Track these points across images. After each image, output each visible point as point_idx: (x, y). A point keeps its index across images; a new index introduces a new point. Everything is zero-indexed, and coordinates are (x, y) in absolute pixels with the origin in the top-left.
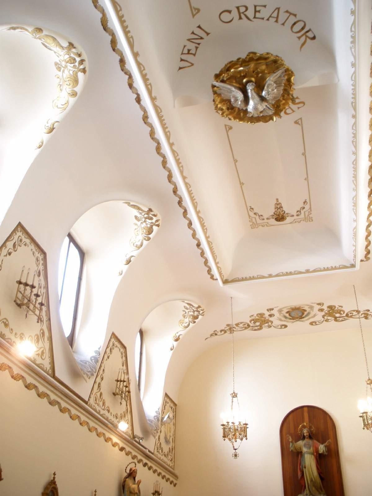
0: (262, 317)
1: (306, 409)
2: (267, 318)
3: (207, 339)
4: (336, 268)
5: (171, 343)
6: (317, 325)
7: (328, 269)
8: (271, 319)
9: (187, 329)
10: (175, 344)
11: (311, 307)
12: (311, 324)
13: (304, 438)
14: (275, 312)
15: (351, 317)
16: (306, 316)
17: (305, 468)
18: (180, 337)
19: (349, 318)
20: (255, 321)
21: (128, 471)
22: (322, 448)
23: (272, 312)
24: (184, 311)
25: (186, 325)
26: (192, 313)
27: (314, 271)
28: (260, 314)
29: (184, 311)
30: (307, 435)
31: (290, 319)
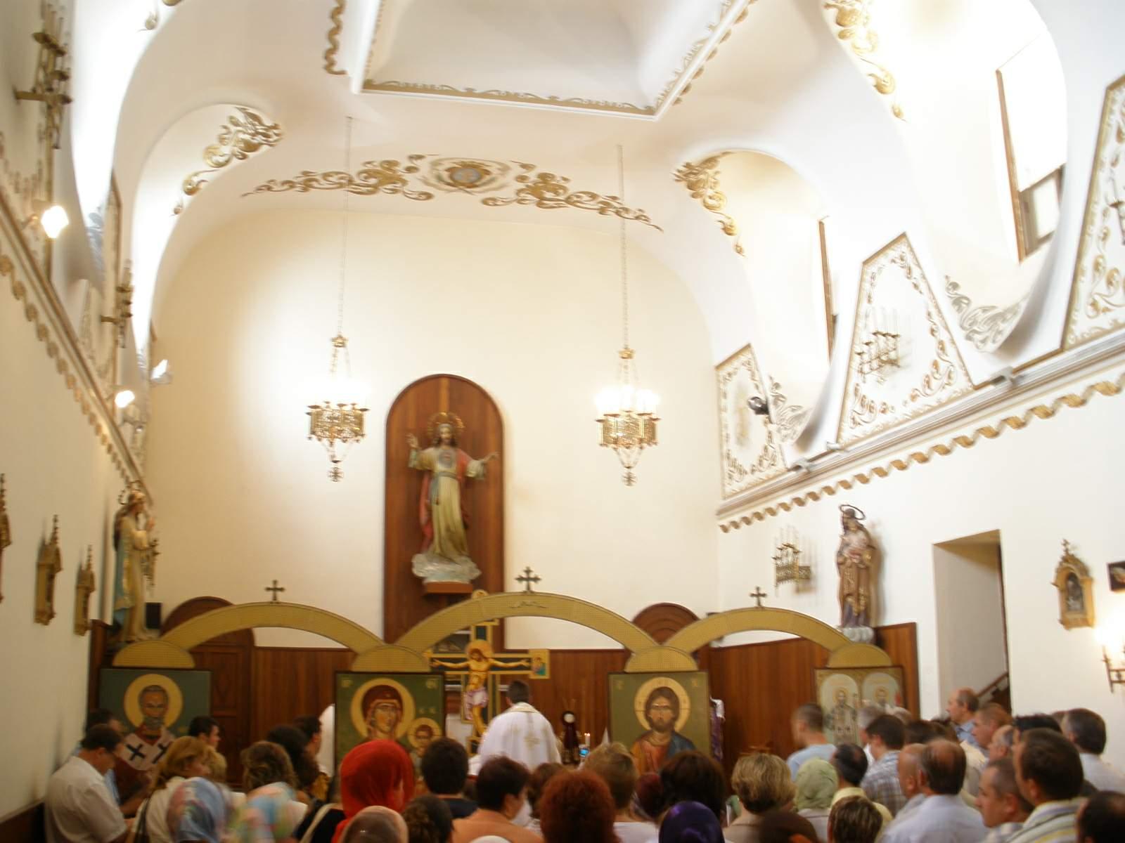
0: (389, 169)
1: (445, 382)
2: (400, 173)
3: (245, 195)
4: (613, 107)
5: (177, 196)
6: (496, 205)
7: (596, 106)
8: (407, 176)
9: (222, 169)
10: (187, 199)
11: (505, 169)
12: (485, 202)
13: (439, 442)
14: (423, 165)
15: (573, 204)
16: (484, 184)
17: (437, 503)
18: (203, 185)
19: (569, 206)
20: (370, 174)
21: (125, 500)
22: (474, 467)
23: (418, 163)
24: (225, 127)
25: (222, 160)
26: (247, 137)
27: (568, 103)
28: (389, 163)
29: (225, 127)
30: (447, 439)
31: (449, 184)
